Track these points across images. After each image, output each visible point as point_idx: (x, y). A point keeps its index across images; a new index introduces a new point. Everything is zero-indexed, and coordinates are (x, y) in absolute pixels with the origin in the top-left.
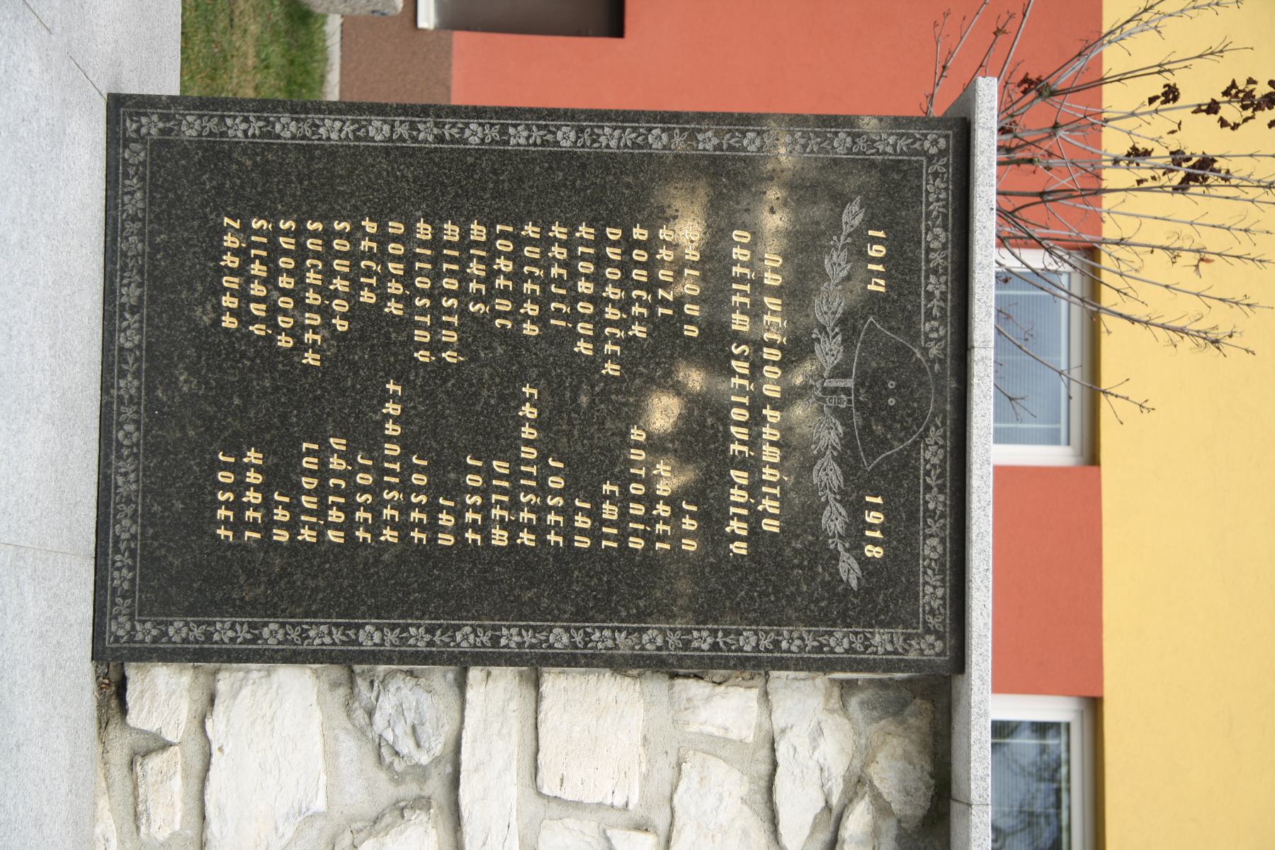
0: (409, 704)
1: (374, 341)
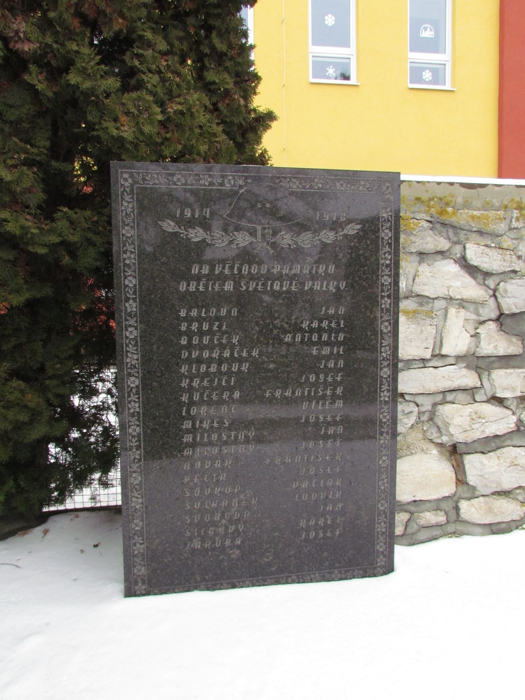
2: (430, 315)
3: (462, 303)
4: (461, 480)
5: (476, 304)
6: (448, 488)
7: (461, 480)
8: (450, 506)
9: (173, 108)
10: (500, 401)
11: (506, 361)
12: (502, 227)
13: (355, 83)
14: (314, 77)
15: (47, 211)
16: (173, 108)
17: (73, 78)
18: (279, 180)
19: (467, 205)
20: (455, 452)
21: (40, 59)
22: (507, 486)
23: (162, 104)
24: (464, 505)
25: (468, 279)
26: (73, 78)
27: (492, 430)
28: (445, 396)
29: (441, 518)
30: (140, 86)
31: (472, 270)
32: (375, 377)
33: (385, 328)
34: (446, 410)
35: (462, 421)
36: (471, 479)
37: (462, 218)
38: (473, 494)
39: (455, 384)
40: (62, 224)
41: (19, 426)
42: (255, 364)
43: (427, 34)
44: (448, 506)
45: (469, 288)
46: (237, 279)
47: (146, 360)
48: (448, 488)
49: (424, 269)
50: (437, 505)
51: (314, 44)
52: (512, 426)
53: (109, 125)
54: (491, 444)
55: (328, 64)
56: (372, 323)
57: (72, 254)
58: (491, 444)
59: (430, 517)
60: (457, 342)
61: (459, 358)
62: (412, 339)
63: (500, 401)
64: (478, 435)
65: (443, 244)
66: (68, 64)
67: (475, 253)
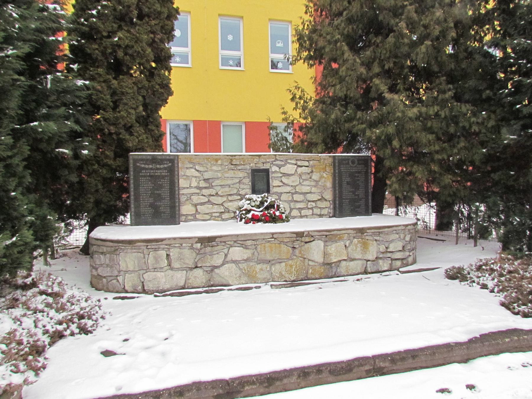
0: (183, 199)
1: (152, 205)
2: (188, 179)
3: (196, 177)
4: (197, 210)
5: (199, 177)
6: (194, 212)
7: (197, 210)
8: (194, 215)
9: (140, 138)
10: (204, 196)
11: (205, 188)
12: (203, 163)
13: (243, 69)
14: (222, 65)
15: (115, 159)
16: (140, 138)
17: (121, 136)
18: (29, 260)
19: (195, 159)
20: (195, 205)
21: (116, 133)
22: (207, 212)
23: (138, 138)
24: (197, 216)
25: (197, 172)
26: (121, 136)
27: (202, 201)
28: (192, 194)
29: (193, 218)
30: (133, 135)
31: (198, 171)
32: (175, 189)
33: (176, 181)
34: (192, 197)
35: (195, 199)
36: (199, 211)
37: (195, 161)
38: (199, 213)
39: (193, 192)
40: (118, 162)
41: (109, 201)
42: (153, 187)
43: (280, 45)
44: (194, 215)
45: (197, 174)
46: (150, 173)
47: (134, 186)
48: (194, 212)
49: (188, 170)
50: (191, 215)
51: (222, 49)
52: (207, 200)
53: (128, 144)
54: (202, 204)
55: (230, 59)
56: (174, 180)
57: (120, 168)
58: (202, 204)
59: (190, 217)
60: (194, 184)
61: (195, 187)
62: (183, 183)
63: (204, 196)
64: (199, 202)
65: (191, 166)
66: (120, 134)
67: (197, 167)
